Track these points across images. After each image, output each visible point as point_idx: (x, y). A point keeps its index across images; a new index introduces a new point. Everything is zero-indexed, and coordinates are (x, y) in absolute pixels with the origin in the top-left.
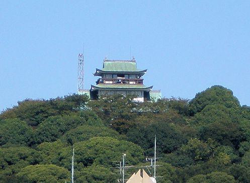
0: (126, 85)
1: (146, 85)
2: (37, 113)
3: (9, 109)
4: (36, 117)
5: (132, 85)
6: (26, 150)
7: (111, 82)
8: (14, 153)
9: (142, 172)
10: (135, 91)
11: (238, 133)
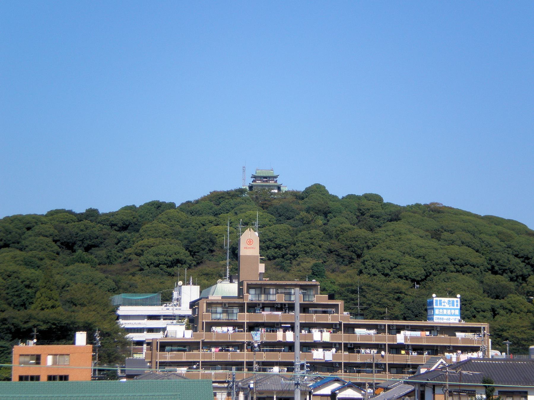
1: (279, 183)
2: (220, 198)
5: (272, 183)
11: (327, 209)
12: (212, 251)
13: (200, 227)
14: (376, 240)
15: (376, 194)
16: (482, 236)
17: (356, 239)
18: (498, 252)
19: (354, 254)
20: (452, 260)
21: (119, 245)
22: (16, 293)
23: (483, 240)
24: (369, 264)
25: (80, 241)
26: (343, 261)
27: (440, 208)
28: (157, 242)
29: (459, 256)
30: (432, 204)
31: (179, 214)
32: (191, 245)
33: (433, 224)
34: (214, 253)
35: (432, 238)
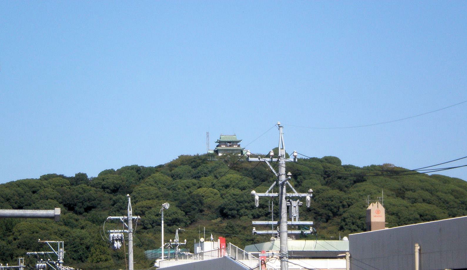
0: (232, 147)
1: (242, 147)
2: (192, 162)
3: (171, 161)
4: (192, 164)
5: (235, 147)
6: (194, 181)
7: (225, 146)
8: (190, 182)
9: (378, 203)
10: (236, 150)
11: (297, 172)
12: (201, 211)
13: (185, 189)
14: (350, 200)
15: (335, 157)
16: (439, 194)
17: (332, 199)
18: (454, 208)
19: (330, 212)
20: (421, 216)
21: (115, 206)
22: (74, 249)
23: (441, 197)
24: (349, 221)
25: (80, 202)
26: (321, 218)
27: (393, 168)
28: (155, 203)
29: (427, 212)
30: (386, 165)
31: (164, 178)
32: (182, 205)
33: (394, 183)
34: (203, 213)
35: (397, 196)
